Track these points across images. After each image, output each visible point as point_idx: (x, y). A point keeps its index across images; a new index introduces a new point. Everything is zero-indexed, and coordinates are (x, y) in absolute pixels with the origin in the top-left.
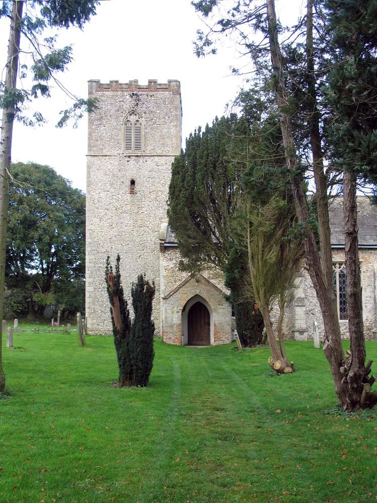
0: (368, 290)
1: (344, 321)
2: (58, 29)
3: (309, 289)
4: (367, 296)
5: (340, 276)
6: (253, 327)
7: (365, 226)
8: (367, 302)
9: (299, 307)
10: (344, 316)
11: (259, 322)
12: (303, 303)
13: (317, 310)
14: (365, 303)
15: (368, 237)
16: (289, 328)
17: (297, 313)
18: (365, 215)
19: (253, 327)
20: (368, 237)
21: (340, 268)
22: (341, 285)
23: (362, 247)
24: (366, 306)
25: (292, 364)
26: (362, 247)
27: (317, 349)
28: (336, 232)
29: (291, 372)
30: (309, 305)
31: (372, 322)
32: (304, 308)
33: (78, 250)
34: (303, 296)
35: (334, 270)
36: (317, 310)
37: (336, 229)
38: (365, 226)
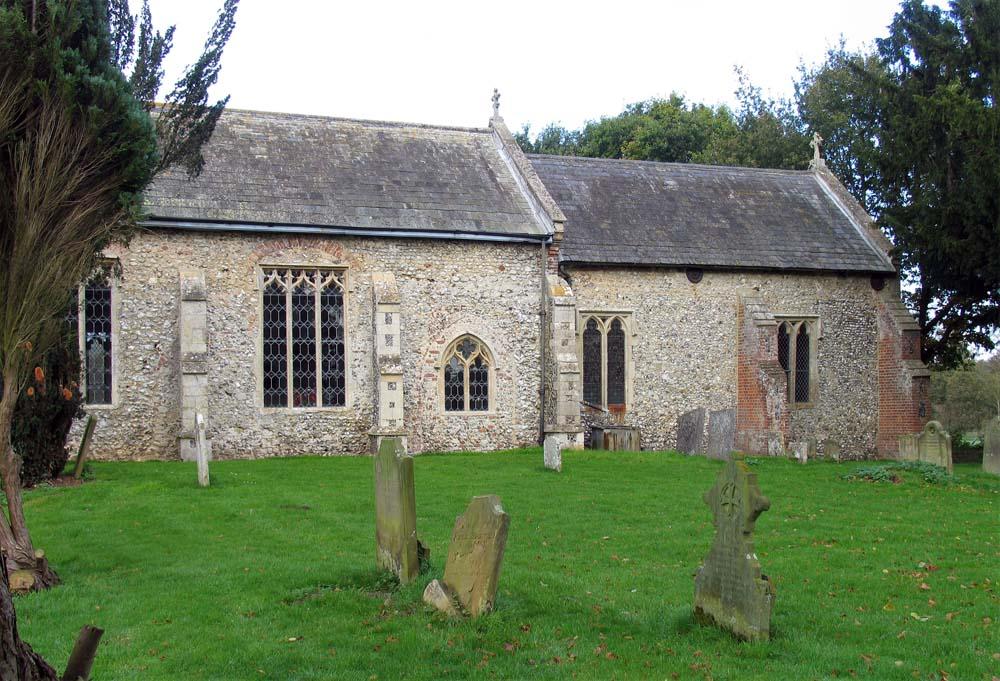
0: (359, 335)
1: (303, 409)
2: (658, 94)
3: (219, 333)
4: (356, 349)
5: (295, 301)
6: (34, 431)
7: (356, 186)
8: (357, 363)
9: (193, 376)
10: (304, 398)
11: (51, 417)
12: (201, 367)
13: (238, 385)
14: (353, 366)
15: (361, 210)
16: (168, 429)
17: (186, 391)
18: (359, 162)
19: (34, 431)
20: (361, 210)
21: (294, 281)
22: (296, 324)
23: (347, 232)
24: (354, 373)
25: (40, 561)
26: (347, 232)
27: (203, 487)
28: (289, 196)
29: (33, 587)
30: (221, 372)
31: (367, 412)
32: (204, 380)
33: (900, 260)
34: (203, 348)
35: (339, 288)
36: (238, 385)
37: (290, 189)
38: (356, 186)
